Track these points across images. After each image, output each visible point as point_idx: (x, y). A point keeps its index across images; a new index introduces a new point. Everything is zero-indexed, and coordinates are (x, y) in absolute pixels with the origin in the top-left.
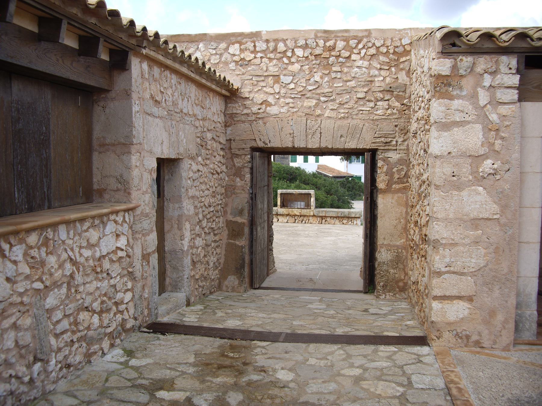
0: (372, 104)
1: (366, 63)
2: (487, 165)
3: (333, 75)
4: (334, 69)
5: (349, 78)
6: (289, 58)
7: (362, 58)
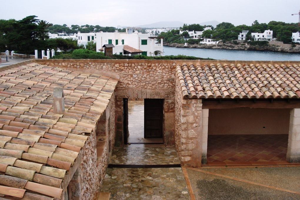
0: (163, 85)
1: (161, 71)
2: (195, 125)
3: (151, 75)
4: (151, 73)
5: (156, 76)
6: (136, 69)
7: (160, 70)
